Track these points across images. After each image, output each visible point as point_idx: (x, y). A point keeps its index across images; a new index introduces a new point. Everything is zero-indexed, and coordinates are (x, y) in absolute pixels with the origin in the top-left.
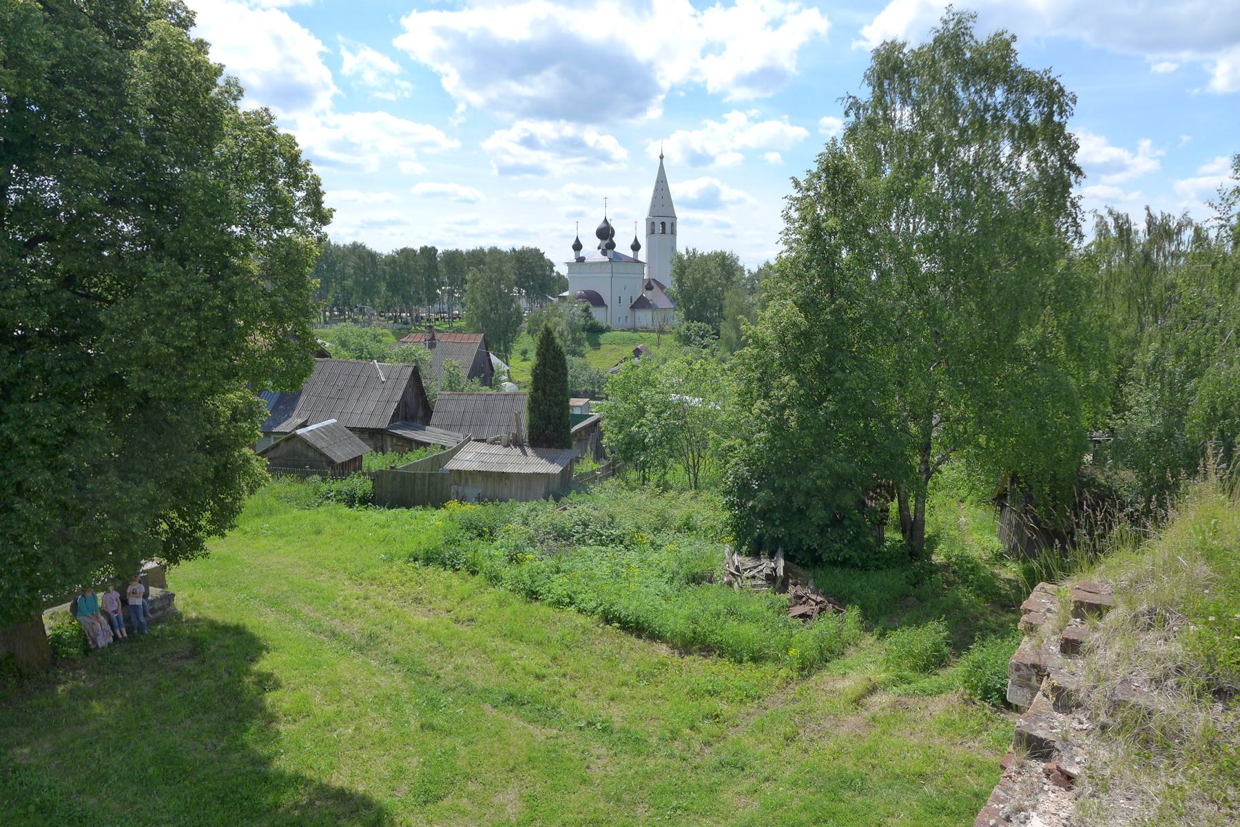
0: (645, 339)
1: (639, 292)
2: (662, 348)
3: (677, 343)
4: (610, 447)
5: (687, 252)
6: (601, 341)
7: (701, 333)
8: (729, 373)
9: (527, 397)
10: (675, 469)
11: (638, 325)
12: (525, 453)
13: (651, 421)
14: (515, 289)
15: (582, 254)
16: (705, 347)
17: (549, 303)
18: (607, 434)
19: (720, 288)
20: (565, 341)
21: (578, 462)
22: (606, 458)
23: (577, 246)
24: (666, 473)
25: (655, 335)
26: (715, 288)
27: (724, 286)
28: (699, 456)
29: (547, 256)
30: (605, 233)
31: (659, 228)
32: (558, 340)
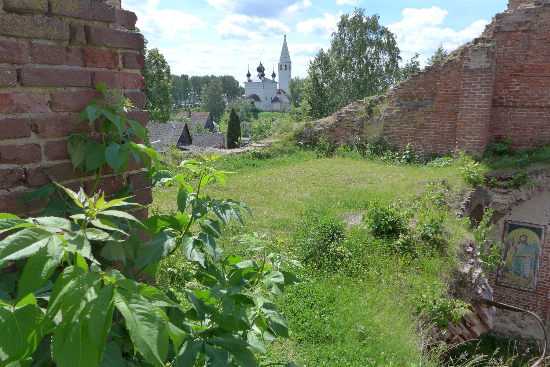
1: (275, 95)
11: (274, 109)
15: (251, 78)
17: (237, 100)
23: (249, 75)
25: (281, 113)
29: (236, 79)
30: (261, 69)
31: (284, 67)
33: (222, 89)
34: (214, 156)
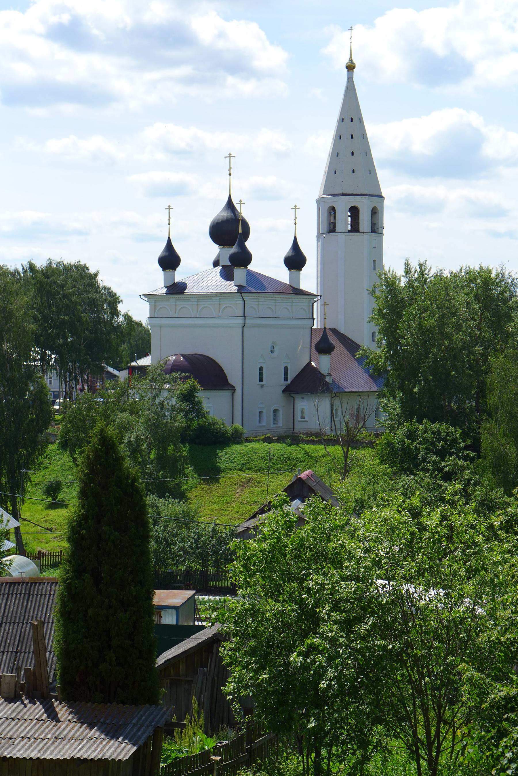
0: (316, 460)
2: (352, 479)
3: (385, 468)
4: (241, 700)
5: (408, 271)
6: (222, 464)
7: (440, 445)
8: (503, 535)
9: (58, 589)
10: (386, 749)
11: (300, 427)
12: (53, 716)
13: (333, 641)
14: (35, 352)
15: (179, 276)
16: (448, 477)
17: (108, 383)
18: (237, 671)
19: (478, 349)
20: (144, 464)
21: (171, 734)
22: (233, 725)
24: (366, 759)
25: (337, 450)
26: (468, 347)
27: (487, 344)
28: (440, 719)
32: (127, 463)
33: (33, 326)
34: (332, 544)
